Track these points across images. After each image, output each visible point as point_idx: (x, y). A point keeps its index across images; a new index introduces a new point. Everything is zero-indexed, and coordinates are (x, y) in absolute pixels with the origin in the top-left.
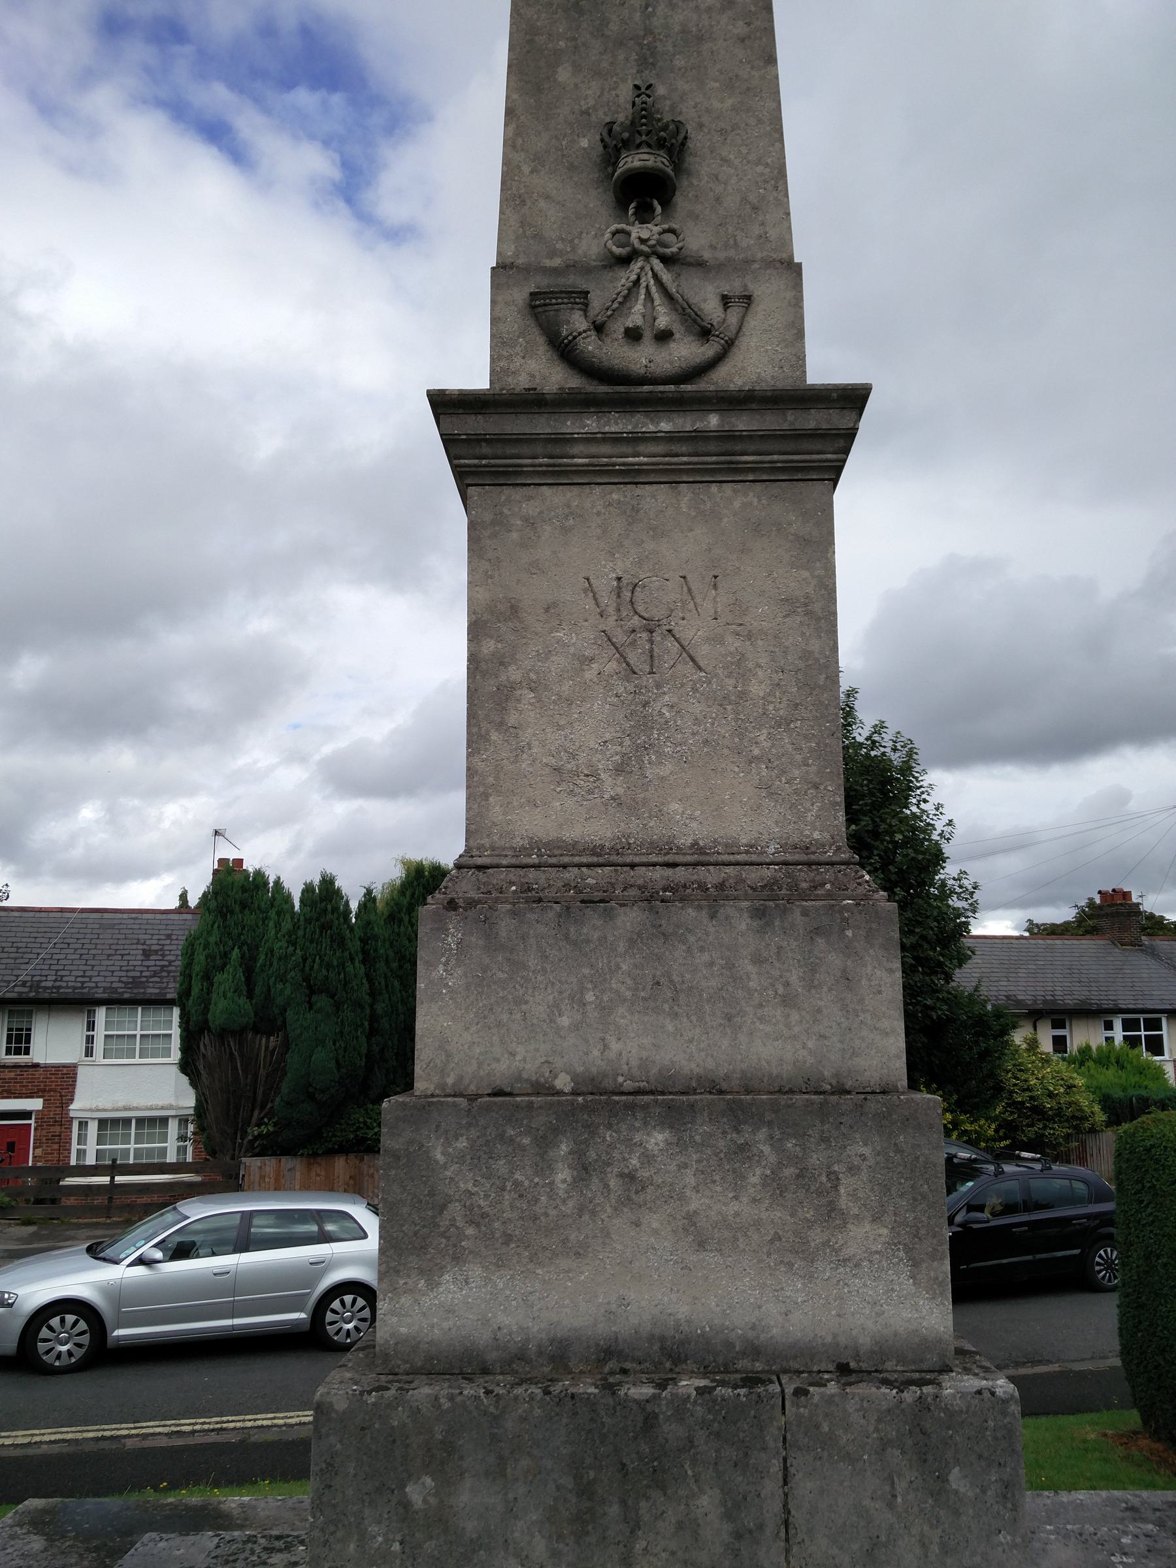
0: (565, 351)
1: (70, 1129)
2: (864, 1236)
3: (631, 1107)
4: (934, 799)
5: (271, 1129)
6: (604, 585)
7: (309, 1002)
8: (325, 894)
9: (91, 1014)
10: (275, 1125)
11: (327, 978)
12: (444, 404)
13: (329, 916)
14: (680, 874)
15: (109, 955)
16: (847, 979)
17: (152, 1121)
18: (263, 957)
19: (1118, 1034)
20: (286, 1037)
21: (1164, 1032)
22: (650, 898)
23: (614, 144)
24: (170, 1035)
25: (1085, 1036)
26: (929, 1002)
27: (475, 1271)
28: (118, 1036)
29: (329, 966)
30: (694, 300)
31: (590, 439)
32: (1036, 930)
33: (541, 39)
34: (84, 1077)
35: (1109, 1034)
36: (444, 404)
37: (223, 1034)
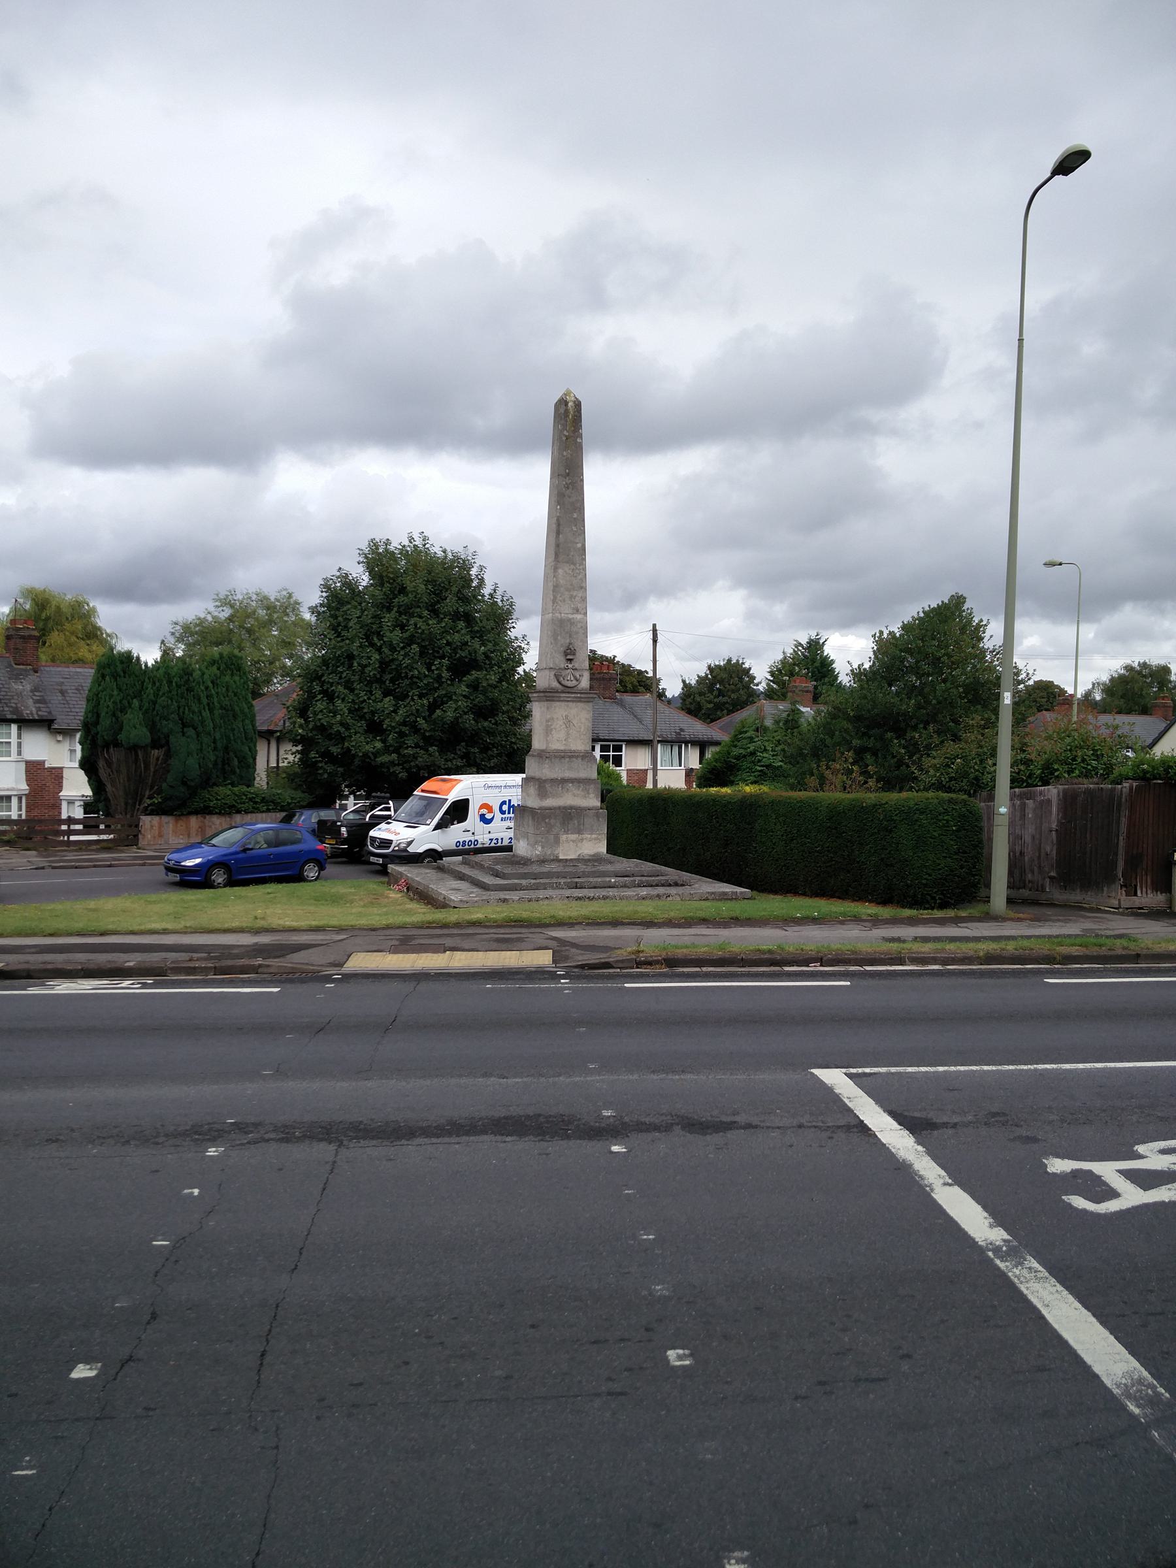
2: (592, 795)
20: (169, 750)
21: (623, 753)
29: (193, 712)
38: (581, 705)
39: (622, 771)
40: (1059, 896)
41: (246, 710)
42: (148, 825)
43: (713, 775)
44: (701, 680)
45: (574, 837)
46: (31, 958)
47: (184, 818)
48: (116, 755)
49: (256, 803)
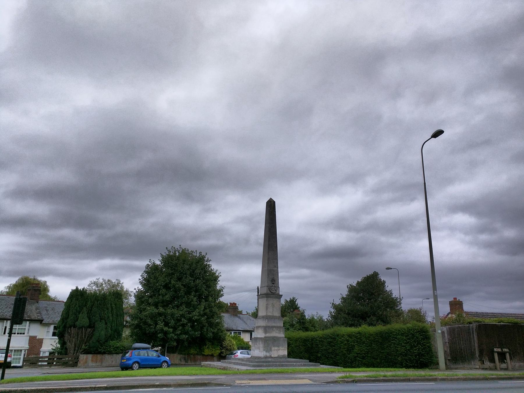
40: (452, 366)
45: (276, 348)
46: (123, 383)
47: (95, 355)
48: (73, 331)
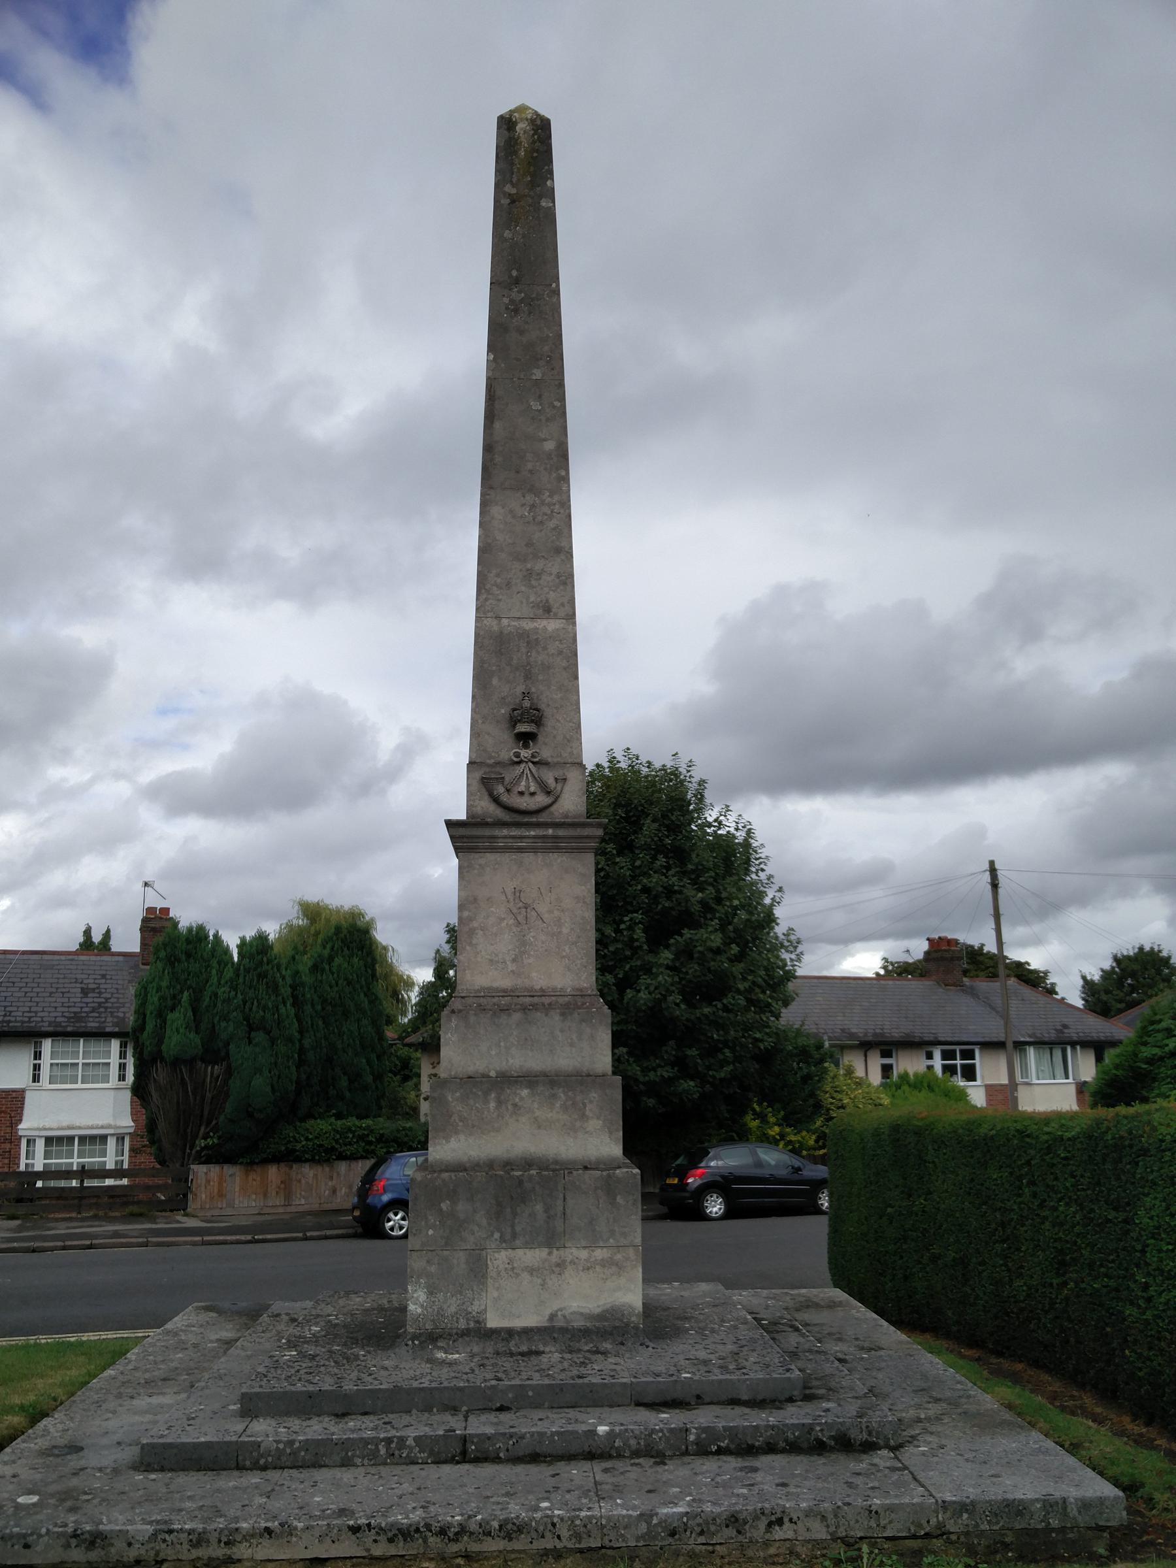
0: (496, 800)
1: (19, 1146)
2: (594, 1124)
3: (516, 1082)
4: (769, 870)
5: (216, 1141)
6: (509, 891)
7: (249, 1038)
8: (257, 948)
9: (38, 1045)
10: (219, 1138)
11: (263, 1017)
12: (450, 824)
13: (265, 967)
14: (536, 1000)
15: (51, 993)
16: (592, 1038)
17: (93, 1139)
18: (208, 999)
19: (938, 1063)
20: (229, 1067)
21: (977, 1061)
22: (524, 1009)
23: (513, 722)
24: (109, 1064)
25: (910, 1065)
26: (758, 1035)
27: (462, 1137)
28: (94, 1064)
29: (265, 1008)
30: (544, 778)
31: (505, 837)
32: (890, 968)
33: (486, 666)
34: (32, 1101)
35: (930, 1062)
36: (450, 824)
37: (176, 1063)
38: (558, 860)
39: (977, 1096)
41: (366, 1005)
42: (201, 1179)
43: (1110, 1091)
44: (1106, 975)
49: (370, 1143)
